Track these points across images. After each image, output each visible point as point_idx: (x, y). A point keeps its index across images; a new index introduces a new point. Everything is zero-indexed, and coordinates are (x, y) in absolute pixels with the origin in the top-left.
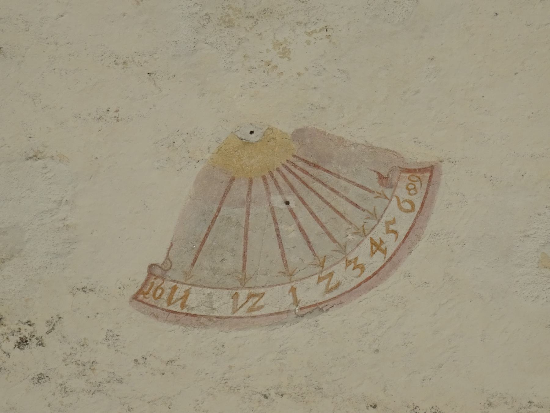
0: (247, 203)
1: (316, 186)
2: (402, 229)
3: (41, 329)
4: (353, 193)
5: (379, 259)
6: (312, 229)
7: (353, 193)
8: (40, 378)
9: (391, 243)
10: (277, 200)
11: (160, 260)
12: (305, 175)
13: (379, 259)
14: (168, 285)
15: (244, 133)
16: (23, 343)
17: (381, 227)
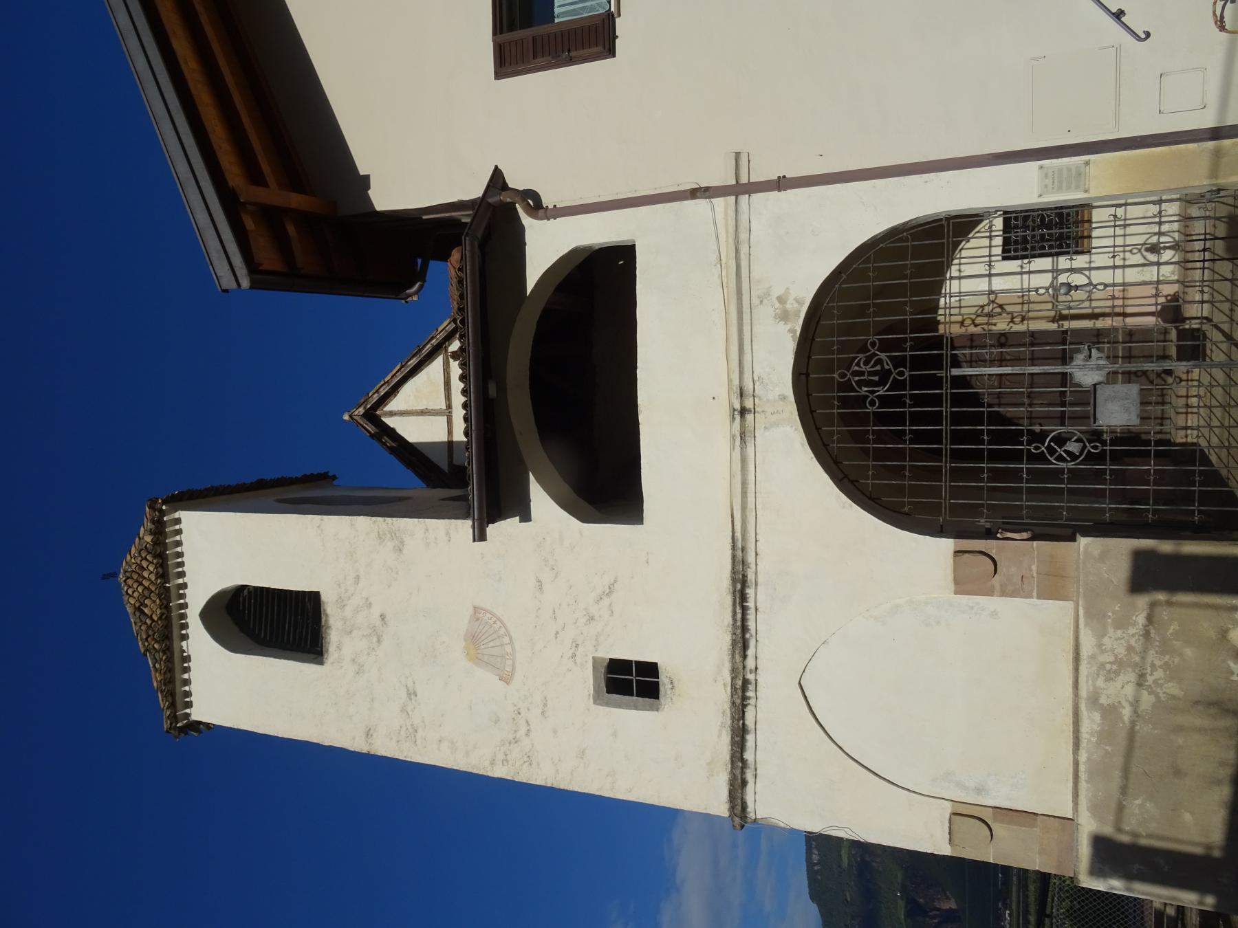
0: (483, 654)
1: (479, 636)
2: (490, 616)
3: (515, 708)
4: (481, 627)
5: (498, 622)
6: (490, 638)
7: (481, 627)
8: (529, 709)
9: (494, 619)
10: (483, 647)
11: (498, 678)
12: (1081, 763)
13: (498, 622)
14: (504, 676)
15: (465, 654)
16: (519, 713)
17: (490, 621)
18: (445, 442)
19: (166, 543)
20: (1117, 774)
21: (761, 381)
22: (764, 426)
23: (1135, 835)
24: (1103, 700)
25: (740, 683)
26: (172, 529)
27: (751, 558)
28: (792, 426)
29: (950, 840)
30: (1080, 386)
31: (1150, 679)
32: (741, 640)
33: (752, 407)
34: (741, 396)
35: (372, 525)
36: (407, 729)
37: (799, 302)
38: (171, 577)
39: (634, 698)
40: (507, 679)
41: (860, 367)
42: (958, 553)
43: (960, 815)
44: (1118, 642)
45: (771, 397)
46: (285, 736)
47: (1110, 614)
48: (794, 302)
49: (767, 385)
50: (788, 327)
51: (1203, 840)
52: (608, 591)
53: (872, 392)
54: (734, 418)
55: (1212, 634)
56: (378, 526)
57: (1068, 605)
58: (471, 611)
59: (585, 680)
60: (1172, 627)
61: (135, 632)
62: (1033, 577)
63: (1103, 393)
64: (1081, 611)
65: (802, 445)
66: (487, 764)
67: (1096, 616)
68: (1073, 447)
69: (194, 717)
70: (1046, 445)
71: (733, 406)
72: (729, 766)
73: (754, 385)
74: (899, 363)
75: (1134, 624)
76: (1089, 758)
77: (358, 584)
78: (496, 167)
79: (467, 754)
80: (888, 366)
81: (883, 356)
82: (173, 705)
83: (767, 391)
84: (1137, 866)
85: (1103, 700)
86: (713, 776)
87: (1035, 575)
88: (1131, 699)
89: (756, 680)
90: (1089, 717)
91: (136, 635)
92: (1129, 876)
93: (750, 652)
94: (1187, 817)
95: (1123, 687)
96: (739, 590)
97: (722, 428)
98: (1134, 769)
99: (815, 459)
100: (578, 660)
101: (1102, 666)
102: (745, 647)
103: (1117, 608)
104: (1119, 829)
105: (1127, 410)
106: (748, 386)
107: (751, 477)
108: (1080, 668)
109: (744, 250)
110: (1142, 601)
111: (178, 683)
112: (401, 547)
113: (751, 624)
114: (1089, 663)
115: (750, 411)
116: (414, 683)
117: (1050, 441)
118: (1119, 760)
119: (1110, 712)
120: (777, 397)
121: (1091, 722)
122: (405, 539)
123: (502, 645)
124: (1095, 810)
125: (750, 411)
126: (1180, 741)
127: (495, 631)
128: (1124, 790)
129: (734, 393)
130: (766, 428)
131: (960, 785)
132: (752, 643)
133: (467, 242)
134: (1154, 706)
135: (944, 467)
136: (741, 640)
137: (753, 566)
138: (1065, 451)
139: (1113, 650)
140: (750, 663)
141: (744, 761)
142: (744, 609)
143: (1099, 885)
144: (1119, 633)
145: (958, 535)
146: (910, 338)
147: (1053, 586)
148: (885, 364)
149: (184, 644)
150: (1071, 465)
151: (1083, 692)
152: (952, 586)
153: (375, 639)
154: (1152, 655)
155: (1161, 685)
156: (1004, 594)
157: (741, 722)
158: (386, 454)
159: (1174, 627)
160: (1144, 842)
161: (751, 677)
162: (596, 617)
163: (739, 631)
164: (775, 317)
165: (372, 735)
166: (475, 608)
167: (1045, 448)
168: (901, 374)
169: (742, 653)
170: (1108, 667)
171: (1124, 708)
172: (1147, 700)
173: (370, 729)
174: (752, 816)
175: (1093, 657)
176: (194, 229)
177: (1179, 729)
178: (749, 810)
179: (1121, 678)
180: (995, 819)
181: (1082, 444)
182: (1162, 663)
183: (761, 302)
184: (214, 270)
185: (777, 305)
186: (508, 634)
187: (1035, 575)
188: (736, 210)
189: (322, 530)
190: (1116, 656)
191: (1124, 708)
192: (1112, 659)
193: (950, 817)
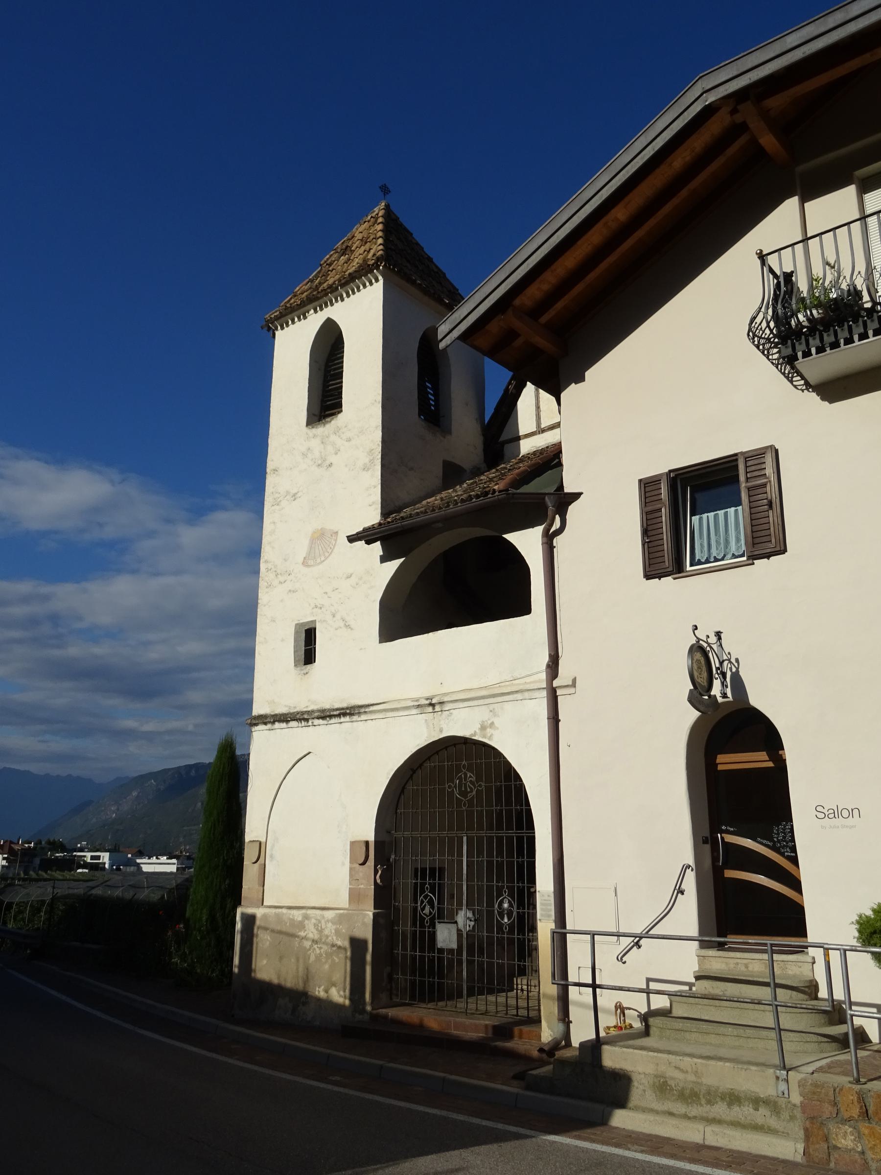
9: (332, 547)
16: (289, 575)
18: (519, 434)
19: (362, 278)
20: (279, 928)
21: (450, 715)
22: (427, 719)
23: (257, 936)
24: (306, 922)
25: (306, 716)
26: (371, 278)
27: (363, 717)
28: (427, 737)
29: (251, 841)
30: (456, 915)
31: (315, 946)
32: (326, 715)
33: (436, 710)
34: (440, 703)
35: (377, 443)
36: (279, 498)
37: (490, 738)
38: (344, 288)
39: (303, 648)
40: (305, 563)
41: (469, 778)
42: (367, 843)
43: (261, 846)
44: (330, 929)
45: (442, 722)
46: (271, 409)
47: (341, 927)
48: (491, 734)
49: (448, 719)
50: (477, 731)
51: (257, 969)
52: (347, 624)
53: (455, 787)
54: (427, 699)
55: (334, 979)
56: (377, 448)
57: (347, 906)
58: (335, 530)
59: (306, 618)
60: (336, 959)
61: (336, 247)
62: (358, 886)
63: (453, 928)
64: (342, 911)
65: (418, 745)
66: (266, 558)
67: (340, 919)
68: (427, 910)
69: (277, 333)
70: (429, 894)
71: (433, 698)
72: (273, 714)
73: (448, 710)
74: (471, 804)
75: (337, 939)
76: (283, 914)
77: (347, 441)
78: (582, 493)
79: (270, 543)
80: (470, 796)
81: (474, 792)
82: (277, 318)
83: (444, 720)
84: (246, 936)
85: (306, 922)
86: (269, 704)
87: (360, 886)
88: (308, 936)
89: (309, 726)
90: (299, 914)
91: (334, 248)
92: (242, 932)
93: (321, 721)
94: (265, 962)
95: (312, 932)
96: (287, 723)
97: (421, 692)
98: (281, 936)
99: (411, 753)
100: (315, 610)
101: (320, 922)
102: (323, 718)
103: (343, 931)
104: (258, 928)
105: (444, 941)
106: (447, 707)
107: (401, 713)
108: (319, 910)
109: (519, 696)
110: (347, 944)
111: (290, 316)
112: (366, 469)
113: (333, 720)
114: (321, 915)
115: (434, 709)
116: (300, 497)
117: (430, 896)
118: (284, 929)
119: (301, 926)
120: (441, 726)
121: (297, 915)
122: (370, 471)
123: (320, 555)
124: (265, 916)
125: (434, 709)
126: (293, 960)
127: (326, 549)
128: (273, 931)
129: (440, 698)
130: (426, 720)
131: (273, 846)
132: (325, 722)
133: (503, 496)
134: (305, 948)
135: (503, 832)
136: (326, 715)
137: (359, 719)
138: (425, 905)
139: (326, 927)
140: (316, 722)
141: (273, 723)
142: (339, 716)
143: (238, 918)
144: (333, 931)
145: (376, 842)
146: (483, 810)
147: (355, 896)
148: (470, 794)
149: (312, 311)
150: (419, 908)
151: (310, 912)
152: (353, 840)
153: (320, 462)
154: (325, 947)
155: (313, 952)
156: (351, 869)
157: (290, 719)
158: (504, 387)
159: (337, 960)
160: (255, 939)
161: (310, 723)
162: (334, 619)
163: (328, 714)
164: (483, 722)
165: (274, 473)
166: (337, 532)
167: (427, 894)
168: (465, 805)
169: (319, 717)
170: (320, 925)
171: (304, 932)
172: (307, 944)
173: (277, 471)
174: (254, 729)
175: (323, 917)
176: (472, 291)
177: (298, 960)
178: (255, 727)
179: (315, 932)
180: (260, 865)
181: (428, 914)
182: (322, 952)
183: (491, 711)
184: (449, 317)
185: (489, 722)
186: (326, 558)
187: (360, 886)
188: (539, 689)
189: (373, 404)
190: (324, 929)
191: (304, 932)
192: (323, 927)
193: (258, 841)
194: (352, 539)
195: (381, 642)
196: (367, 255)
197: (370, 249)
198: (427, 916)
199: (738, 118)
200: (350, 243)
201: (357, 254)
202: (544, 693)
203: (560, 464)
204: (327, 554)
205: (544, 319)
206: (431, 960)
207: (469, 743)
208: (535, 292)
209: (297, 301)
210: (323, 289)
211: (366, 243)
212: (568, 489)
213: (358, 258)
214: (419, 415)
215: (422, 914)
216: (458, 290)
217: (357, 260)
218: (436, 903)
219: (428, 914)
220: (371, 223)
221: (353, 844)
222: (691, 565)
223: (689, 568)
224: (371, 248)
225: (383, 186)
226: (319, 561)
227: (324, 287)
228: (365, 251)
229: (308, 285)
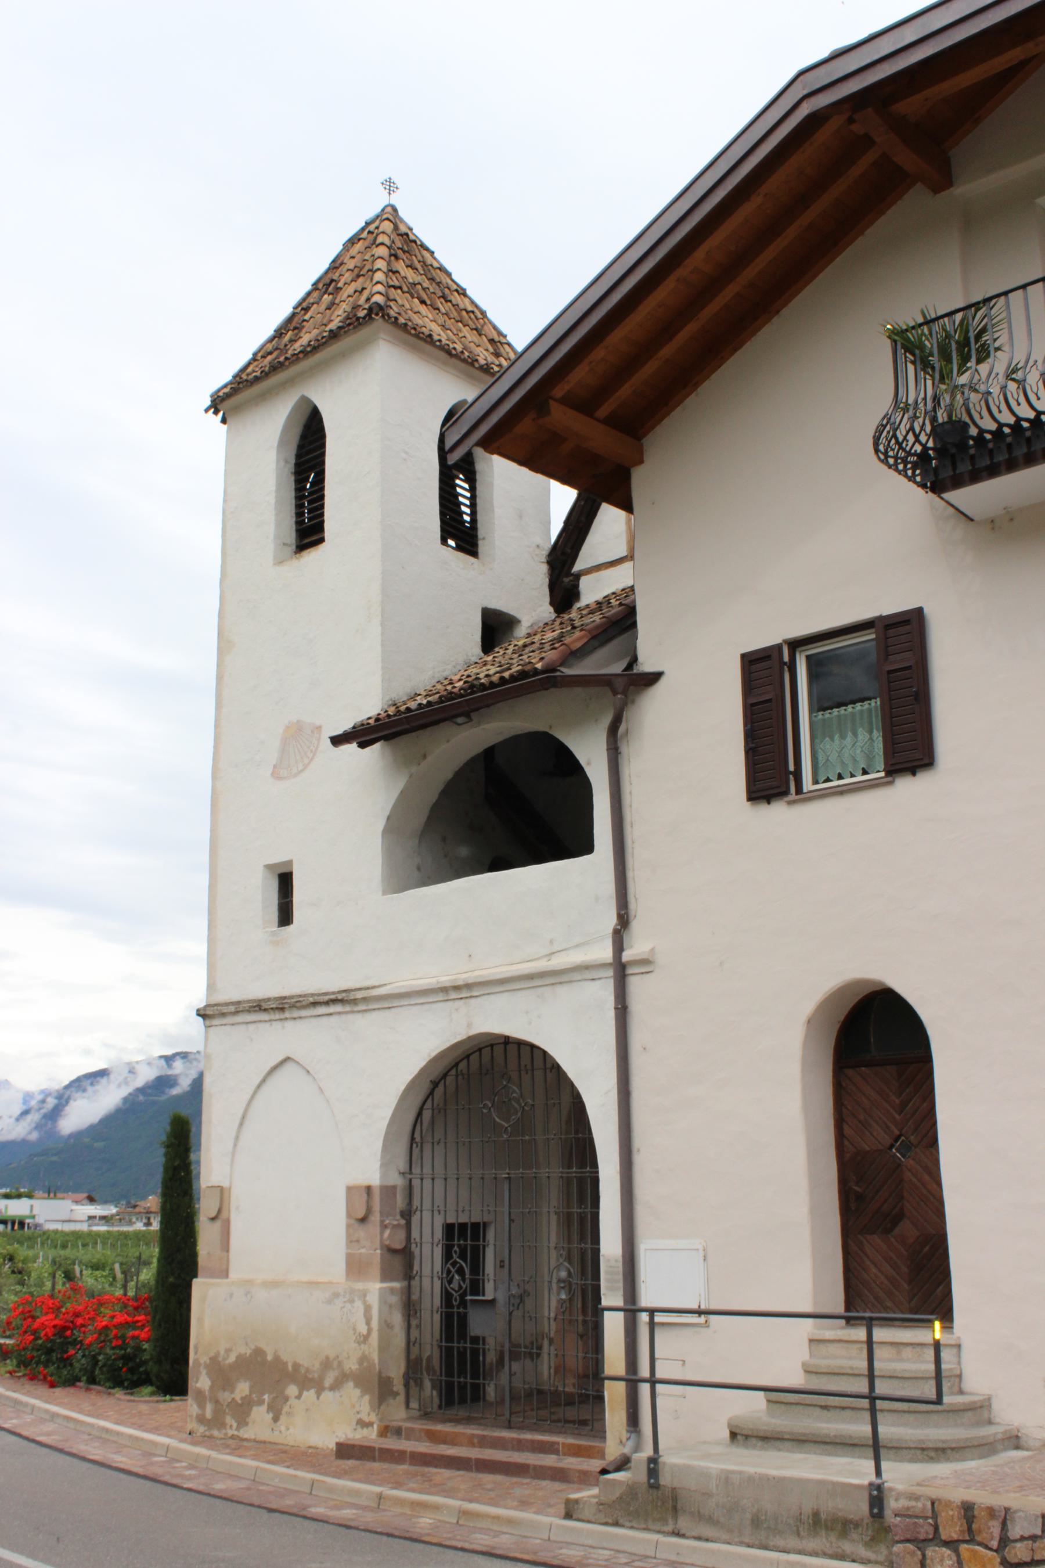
9: (314, 750)
42: (369, 1189)
43: (222, 1193)
58: (318, 723)
59: (278, 858)
117: (460, 1263)
147: (355, 1267)
181: (457, 1289)
186: (306, 766)
193: (219, 1187)
194: (337, 741)
195: (384, 893)
196: (358, 299)
197: (363, 289)
198: (456, 1292)
199: (857, 128)
200: (337, 274)
201: (345, 295)
202: (610, 973)
203: (634, 625)
204: (306, 761)
205: (603, 412)
206: (462, 1354)
207: (511, 1043)
208: (580, 375)
209: (257, 369)
210: (292, 353)
211: (358, 276)
212: (647, 664)
213: (346, 302)
214: (444, 541)
215: (449, 1288)
216: (505, 336)
217: (344, 306)
218: (467, 1271)
219: (457, 1289)
220: (367, 243)
221: (350, 1190)
222: (816, 782)
223: (807, 784)
224: (365, 286)
225: (386, 181)
226: (295, 770)
227: (295, 350)
228: (355, 291)
229: (274, 342)
